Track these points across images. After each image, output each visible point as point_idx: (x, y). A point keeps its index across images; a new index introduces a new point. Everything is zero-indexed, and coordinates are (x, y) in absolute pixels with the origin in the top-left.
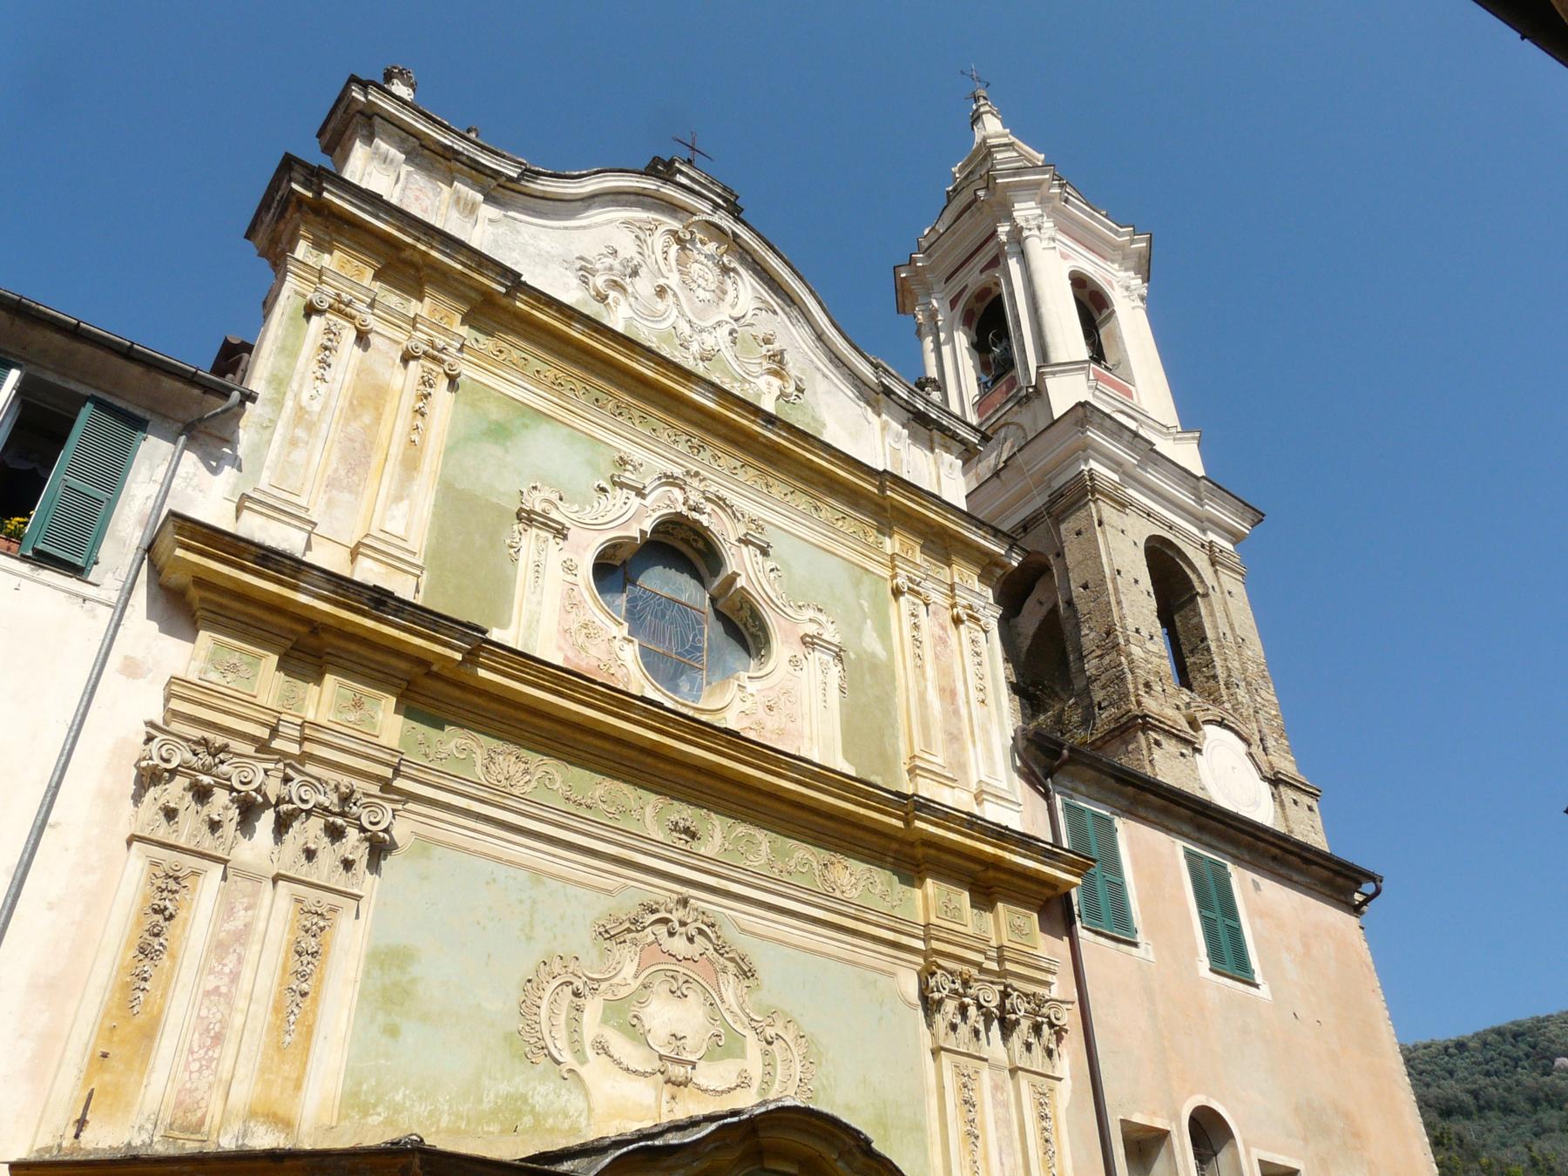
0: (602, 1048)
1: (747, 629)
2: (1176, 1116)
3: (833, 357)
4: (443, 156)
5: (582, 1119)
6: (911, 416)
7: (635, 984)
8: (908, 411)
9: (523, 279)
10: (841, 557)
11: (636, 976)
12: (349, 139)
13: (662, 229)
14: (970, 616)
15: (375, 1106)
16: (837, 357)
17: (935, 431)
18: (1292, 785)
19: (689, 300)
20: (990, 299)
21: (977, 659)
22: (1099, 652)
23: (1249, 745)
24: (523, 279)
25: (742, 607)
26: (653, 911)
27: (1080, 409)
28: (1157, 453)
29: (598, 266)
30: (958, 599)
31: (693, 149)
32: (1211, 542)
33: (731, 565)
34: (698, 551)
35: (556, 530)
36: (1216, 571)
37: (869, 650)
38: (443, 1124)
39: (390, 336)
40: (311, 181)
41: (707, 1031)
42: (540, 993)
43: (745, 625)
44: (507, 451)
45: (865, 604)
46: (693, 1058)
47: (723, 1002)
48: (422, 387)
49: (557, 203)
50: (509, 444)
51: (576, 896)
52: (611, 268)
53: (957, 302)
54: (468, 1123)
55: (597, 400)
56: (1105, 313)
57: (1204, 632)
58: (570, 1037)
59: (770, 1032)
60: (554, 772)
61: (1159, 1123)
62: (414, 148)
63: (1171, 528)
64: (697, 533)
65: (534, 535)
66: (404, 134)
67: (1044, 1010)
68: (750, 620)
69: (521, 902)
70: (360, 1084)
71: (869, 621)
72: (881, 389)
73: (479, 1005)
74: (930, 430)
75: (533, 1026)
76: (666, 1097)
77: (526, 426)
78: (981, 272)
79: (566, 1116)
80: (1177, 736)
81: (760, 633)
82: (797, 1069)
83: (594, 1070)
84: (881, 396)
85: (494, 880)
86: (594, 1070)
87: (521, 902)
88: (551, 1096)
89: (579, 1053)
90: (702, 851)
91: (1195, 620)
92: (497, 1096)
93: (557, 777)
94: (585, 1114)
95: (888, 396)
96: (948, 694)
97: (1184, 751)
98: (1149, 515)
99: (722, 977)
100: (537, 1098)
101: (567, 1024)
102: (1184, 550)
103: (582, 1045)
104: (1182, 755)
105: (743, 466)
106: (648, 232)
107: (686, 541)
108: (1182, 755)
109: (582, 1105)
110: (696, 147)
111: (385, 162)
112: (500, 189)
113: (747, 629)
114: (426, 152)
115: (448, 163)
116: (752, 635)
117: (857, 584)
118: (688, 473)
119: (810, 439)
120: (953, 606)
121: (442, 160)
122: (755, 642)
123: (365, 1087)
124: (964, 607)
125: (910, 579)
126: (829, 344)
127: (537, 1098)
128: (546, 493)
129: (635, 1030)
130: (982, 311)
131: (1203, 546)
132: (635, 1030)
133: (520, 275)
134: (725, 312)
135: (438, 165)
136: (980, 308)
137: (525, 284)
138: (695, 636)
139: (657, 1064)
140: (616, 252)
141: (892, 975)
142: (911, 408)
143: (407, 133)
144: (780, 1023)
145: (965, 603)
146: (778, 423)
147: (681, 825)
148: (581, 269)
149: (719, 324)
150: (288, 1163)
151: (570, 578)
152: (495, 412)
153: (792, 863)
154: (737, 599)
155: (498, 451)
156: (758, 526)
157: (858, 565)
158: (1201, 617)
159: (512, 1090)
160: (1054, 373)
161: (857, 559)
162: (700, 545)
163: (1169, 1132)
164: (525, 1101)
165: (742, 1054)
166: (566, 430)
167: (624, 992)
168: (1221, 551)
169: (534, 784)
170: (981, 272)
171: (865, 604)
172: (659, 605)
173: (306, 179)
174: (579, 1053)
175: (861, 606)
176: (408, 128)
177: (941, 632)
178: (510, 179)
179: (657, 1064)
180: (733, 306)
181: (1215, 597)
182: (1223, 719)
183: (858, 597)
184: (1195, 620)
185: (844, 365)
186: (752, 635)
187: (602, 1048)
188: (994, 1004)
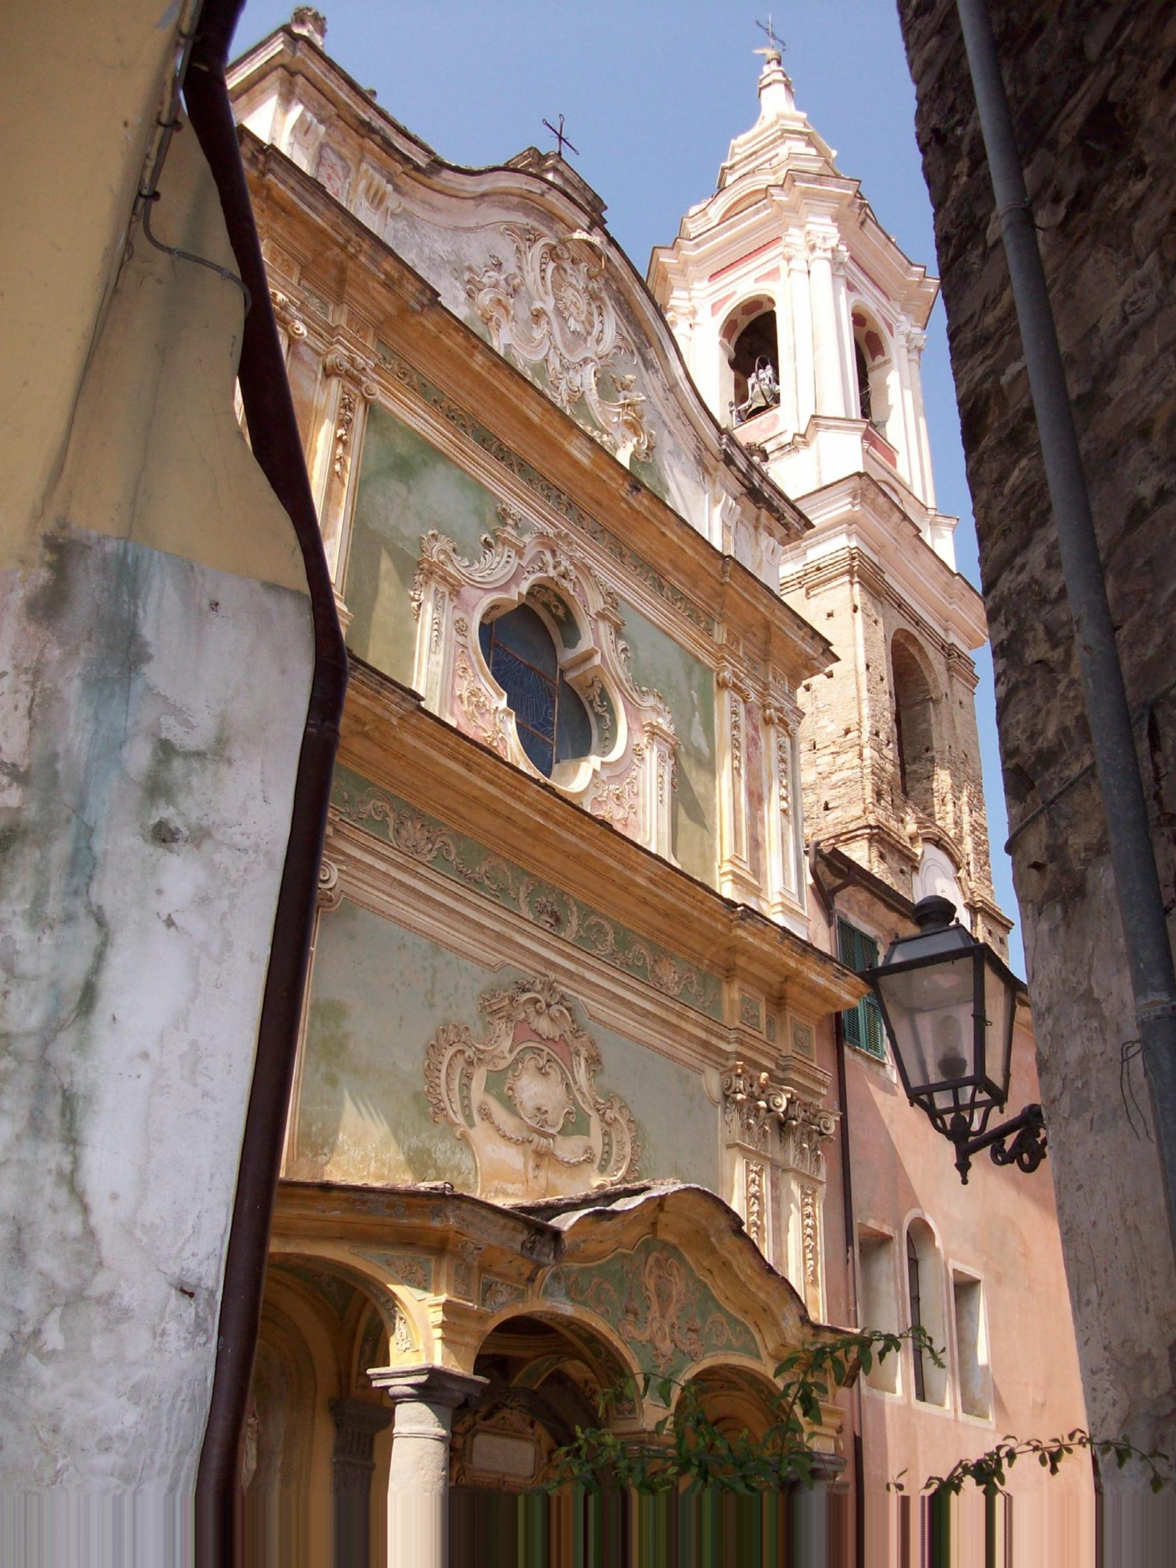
0: (486, 1115)
1: (592, 708)
2: (898, 1226)
3: (681, 413)
4: (356, 131)
5: (471, 1176)
6: (744, 490)
7: (510, 1058)
8: (744, 485)
9: (439, 299)
10: (678, 643)
11: (511, 1051)
12: (262, 92)
13: (542, 242)
14: (780, 720)
15: (322, 1147)
16: (686, 415)
17: (763, 511)
18: (994, 918)
19: (562, 329)
20: (760, 312)
21: (782, 766)
22: (833, 749)
23: (958, 869)
24: (439, 299)
25: (592, 684)
26: (524, 990)
27: (856, 478)
28: (921, 540)
29: (485, 280)
30: (770, 700)
31: (560, 138)
32: (952, 644)
33: (586, 643)
34: (555, 617)
35: (452, 585)
36: (951, 677)
37: (696, 745)
38: (372, 1169)
39: (312, 344)
40: (257, 158)
41: (564, 1108)
42: (440, 1058)
43: (591, 703)
44: (409, 491)
45: (695, 695)
46: (551, 1131)
47: (575, 1083)
48: (343, 411)
49: (454, 200)
50: (411, 482)
51: (466, 969)
52: (495, 285)
53: (720, 308)
54: (390, 1171)
55: (484, 440)
56: (880, 359)
57: (931, 741)
58: (462, 1102)
59: (610, 1114)
60: (450, 843)
61: (887, 1230)
62: (330, 117)
63: (917, 624)
64: (560, 600)
65: (433, 589)
66: (324, 101)
67: (817, 1120)
68: (598, 699)
69: (425, 969)
70: (310, 1125)
71: (697, 714)
72: (722, 456)
73: (394, 1063)
74: (759, 508)
75: (434, 1086)
76: (531, 1164)
77: (425, 464)
78: (757, 280)
79: (460, 1173)
80: (900, 851)
81: (607, 716)
82: (628, 1150)
83: (479, 1133)
84: (722, 465)
85: (404, 946)
86: (479, 1133)
87: (425, 969)
88: (449, 1153)
89: (469, 1118)
90: (562, 935)
91: (924, 726)
92: (409, 1148)
93: (452, 848)
94: (473, 1172)
95: (727, 465)
96: (756, 798)
97: (904, 868)
98: (899, 606)
99: (575, 1059)
100: (439, 1154)
101: (460, 1090)
102: (926, 650)
103: (471, 1112)
104: (902, 872)
105: (602, 531)
106: (528, 243)
107: (546, 605)
108: (902, 872)
109: (471, 1164)
110: (564, 136)
111: (306, 133)
112: (404, 176)
113: (592, 708)
114: (341, 123)
115: (360, 140)
116: (596, 714)
117: (689, 674)
118: (558, 535)
119: (669, 512)
120: (765, 707)
121: (354, 134)
122: (598, 722)
123: (314, 1129)
124: (777, 709)
125: (736, 676)
126: (680, 398)
127: (439, 1154)
128: (443, 543)
129: (510, 1104)
130: (746, 324)
131: (943, 647)
132: (510, 1104)
133: (438, 295)
134: (590, 350)
135: (349, 140)
136: (744, 322)
137: (440, 304)
138: (547, 708)
139: (525, 1134)
140: (501, 264)
141: (701, 1072)
142: (747, 483)
143: (328, 99)
144: (617, 1106)
145: (777, 705)
146: (643, 491)
147: (549, 909)
148: (469, 282)
149: (585, 361)
150: (335, 1194)
151: (461, 639)
152: (402, 447)
153: (630, 956)
154: (590, 677)
155: (402, 489)
156: (614, 600)
157: (690, 653)
158: (930, 725)
159: (421, 1145)
160: (828, 428)
161: (690, 645)
162: (560, 612)
163: (891, 1238)
164: (430, 1156)
165: (587, 1133)
166: (457, 472)
167: (502, 1065)
168: (959, 656)
169: (434, 853)
170: (757, 280)
171: (695, 695)
172: (519, 671)
173: (253, 155)
174: (469, 1118)
175: (691, 696)
176: (330, 96)
177: (753, 732)
178: (417, 168)
179: (525, 1134)
180: (598, 341)
181: (943, 707)
182: (941, 839)
183: (690, 688)
184: (924, 726)
185: (691, 423)
186: (596, 714)
187: (486, 1115)
188: (781, 1110)
